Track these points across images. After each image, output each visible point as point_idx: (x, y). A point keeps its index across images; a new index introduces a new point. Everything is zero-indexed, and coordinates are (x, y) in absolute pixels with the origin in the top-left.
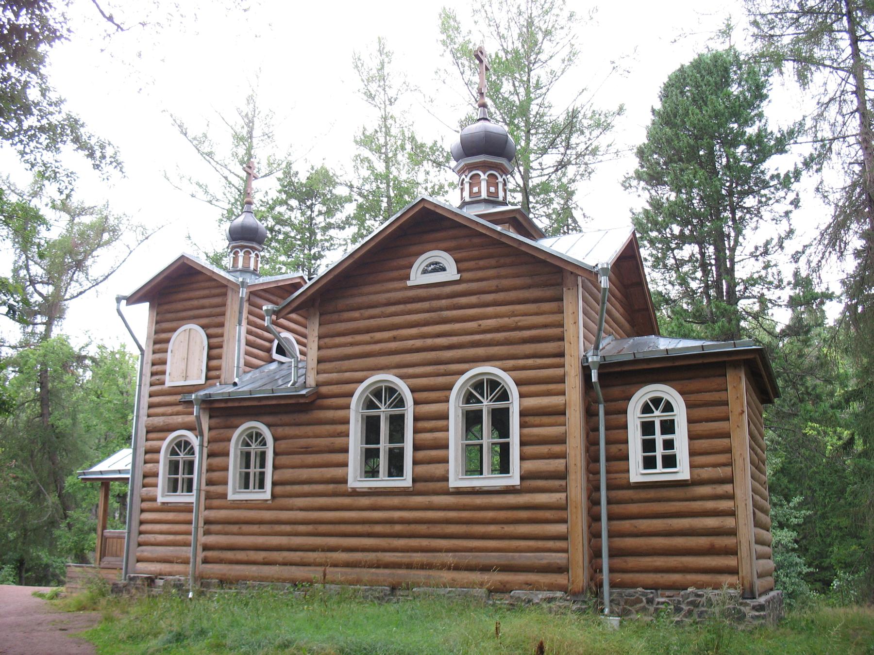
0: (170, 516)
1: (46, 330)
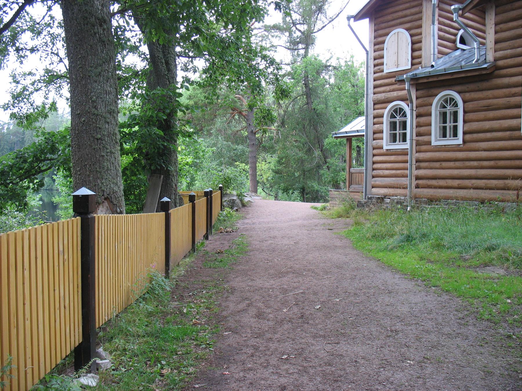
0: (393, 158)
1: (305, 53)
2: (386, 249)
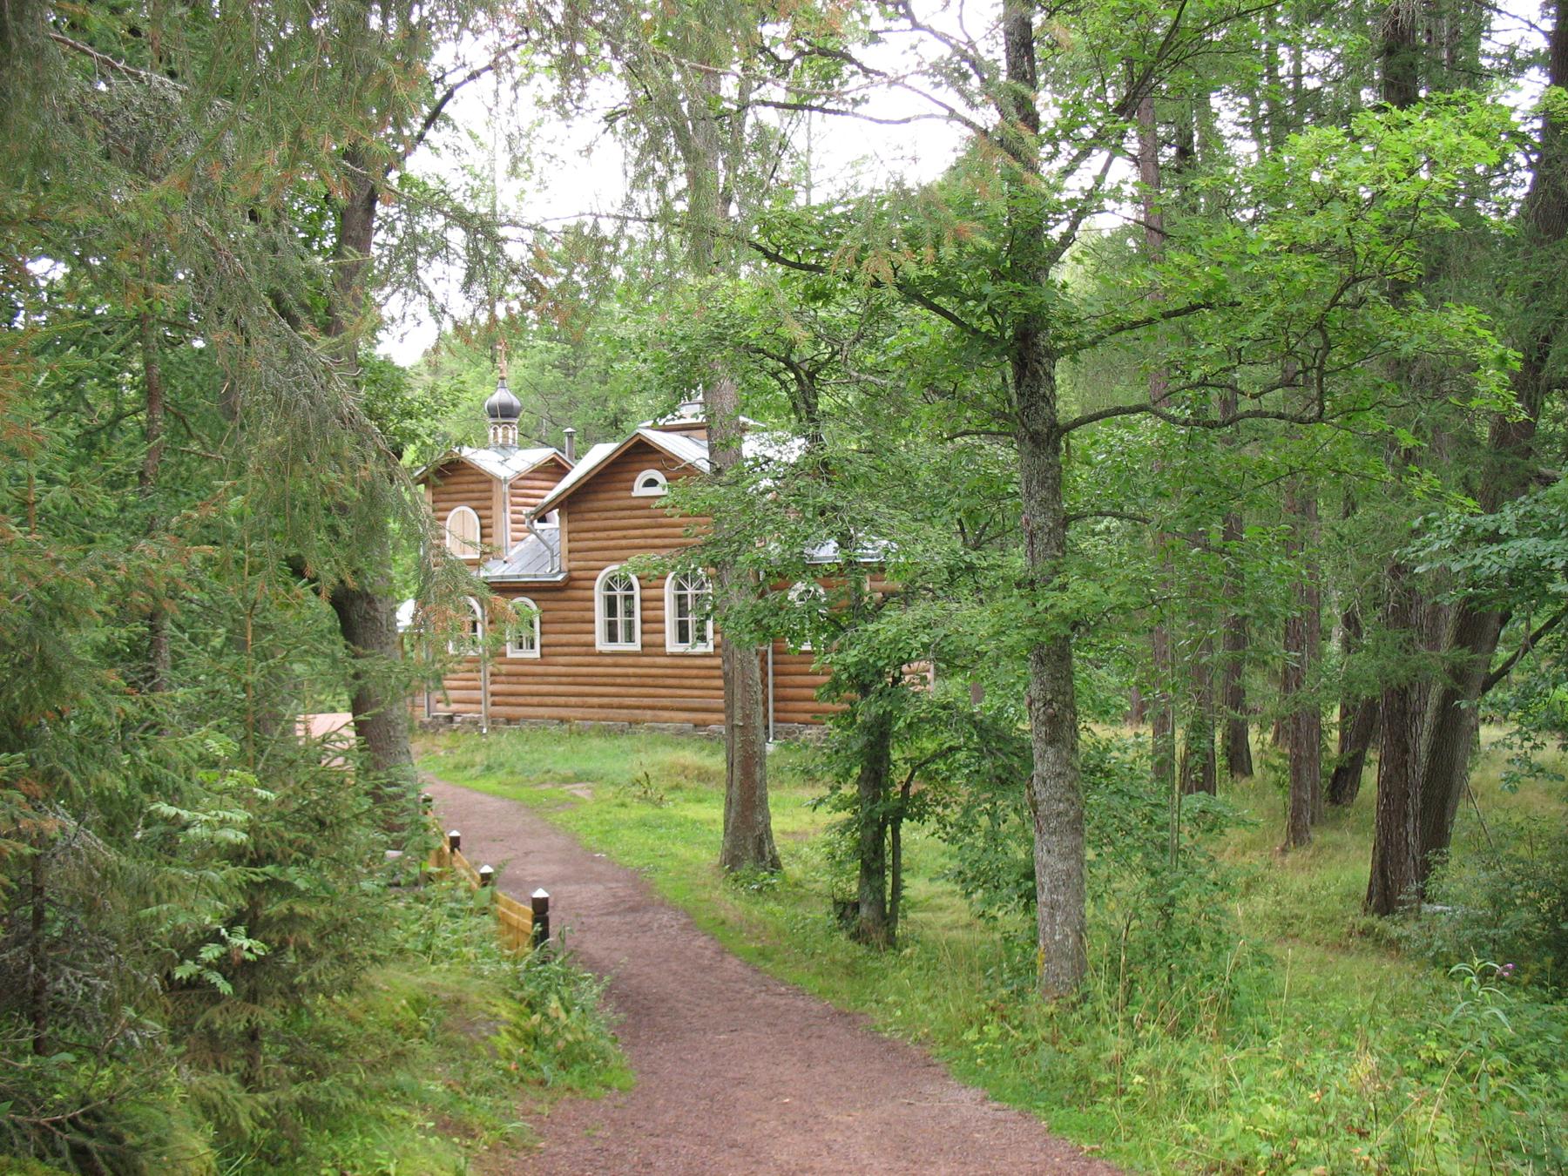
2: (470, 779)
